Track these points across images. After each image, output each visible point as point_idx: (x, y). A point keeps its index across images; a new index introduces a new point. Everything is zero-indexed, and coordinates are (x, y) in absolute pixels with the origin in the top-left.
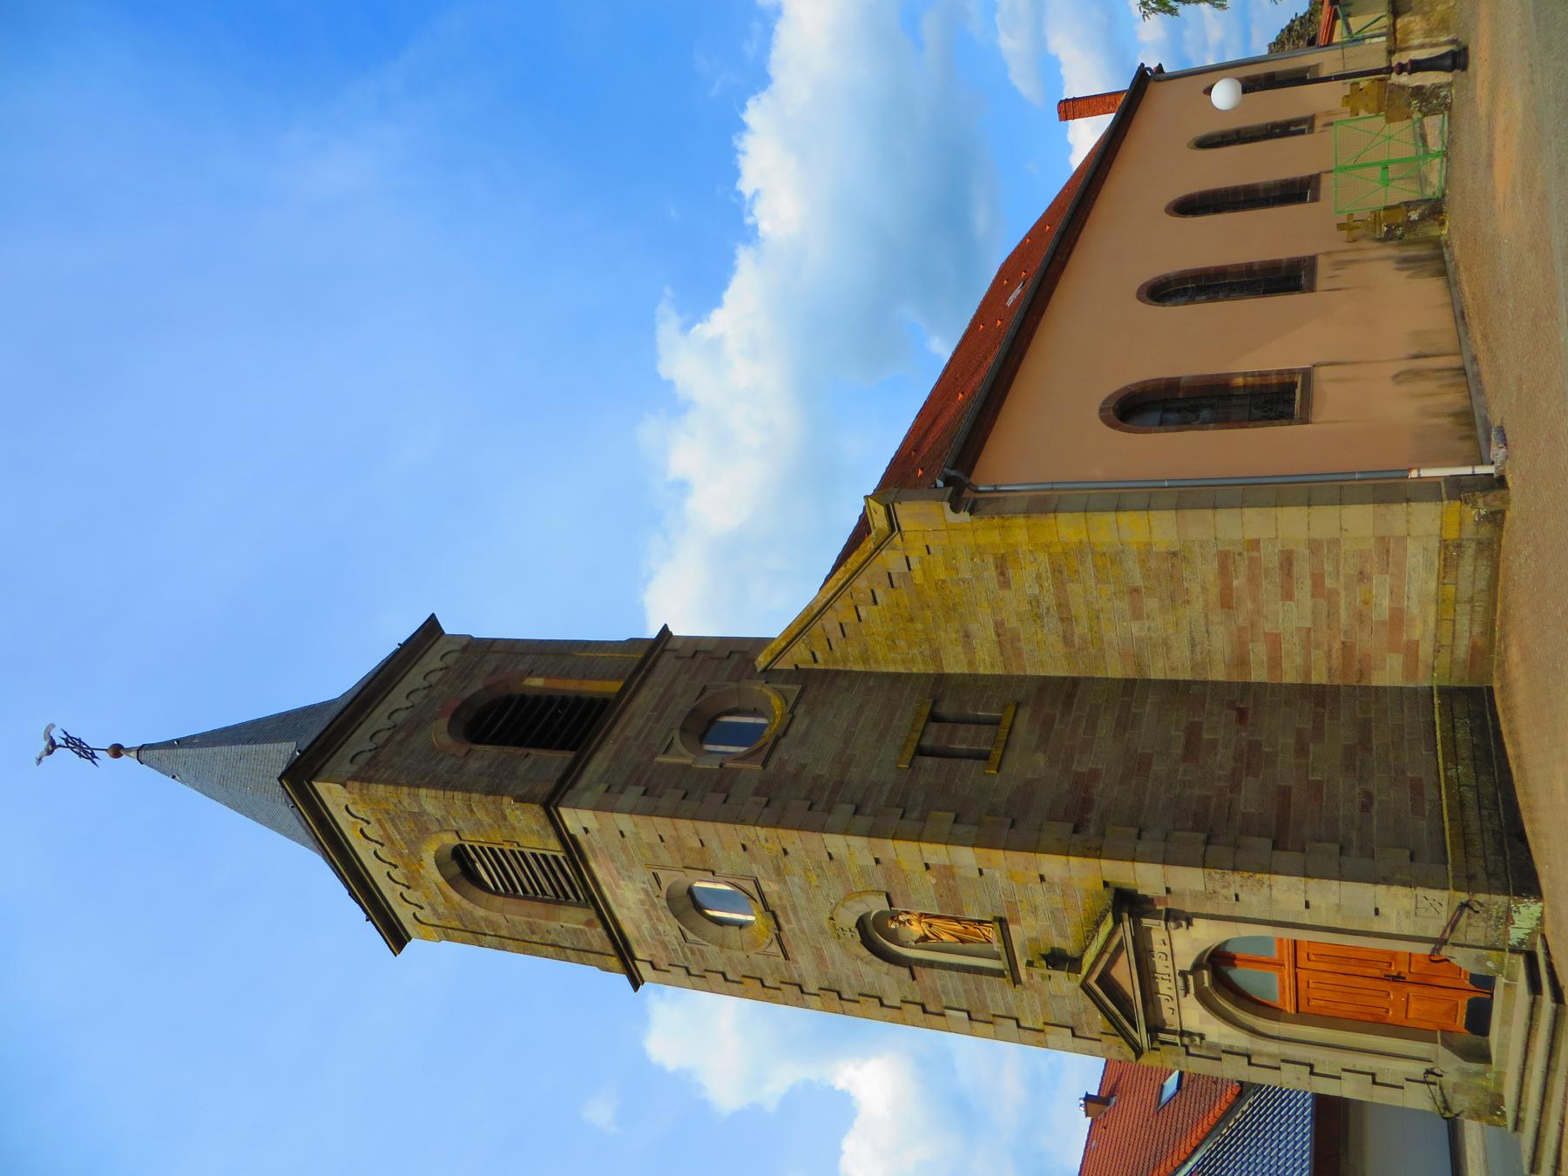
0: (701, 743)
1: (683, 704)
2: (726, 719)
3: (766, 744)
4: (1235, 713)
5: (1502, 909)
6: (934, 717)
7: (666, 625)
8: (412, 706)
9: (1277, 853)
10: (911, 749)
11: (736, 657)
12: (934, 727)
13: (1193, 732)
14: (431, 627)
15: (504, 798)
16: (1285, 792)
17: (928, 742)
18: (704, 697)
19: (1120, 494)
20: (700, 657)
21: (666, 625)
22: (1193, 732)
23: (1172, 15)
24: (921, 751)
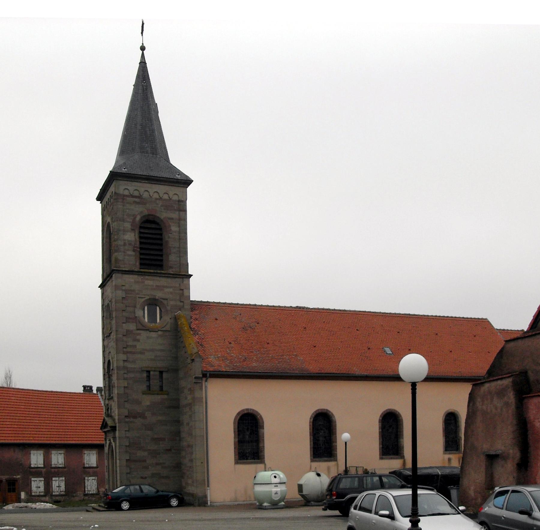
0: (147, 305)
1: (159, 295)
2: (158, 308)
3: (145, 327)
4: (169, 448)
5: (465, 466)
6: (161, 373)
7: (192, 275)
8: (151, 197)
9: (125, 460)
10: (149, 369)
11: (182, 304)
12: (157, 373)
13: (163, 439)
14: (187, 182)
15: (31, 463)
16: (145, 461)
17: (152, 373)
18: (162, 300)
19: (203, 436)
20: (181, 292)
21: (192, 275)
22: (163, 439)
23: (366, 470)
24: (148, 372)
